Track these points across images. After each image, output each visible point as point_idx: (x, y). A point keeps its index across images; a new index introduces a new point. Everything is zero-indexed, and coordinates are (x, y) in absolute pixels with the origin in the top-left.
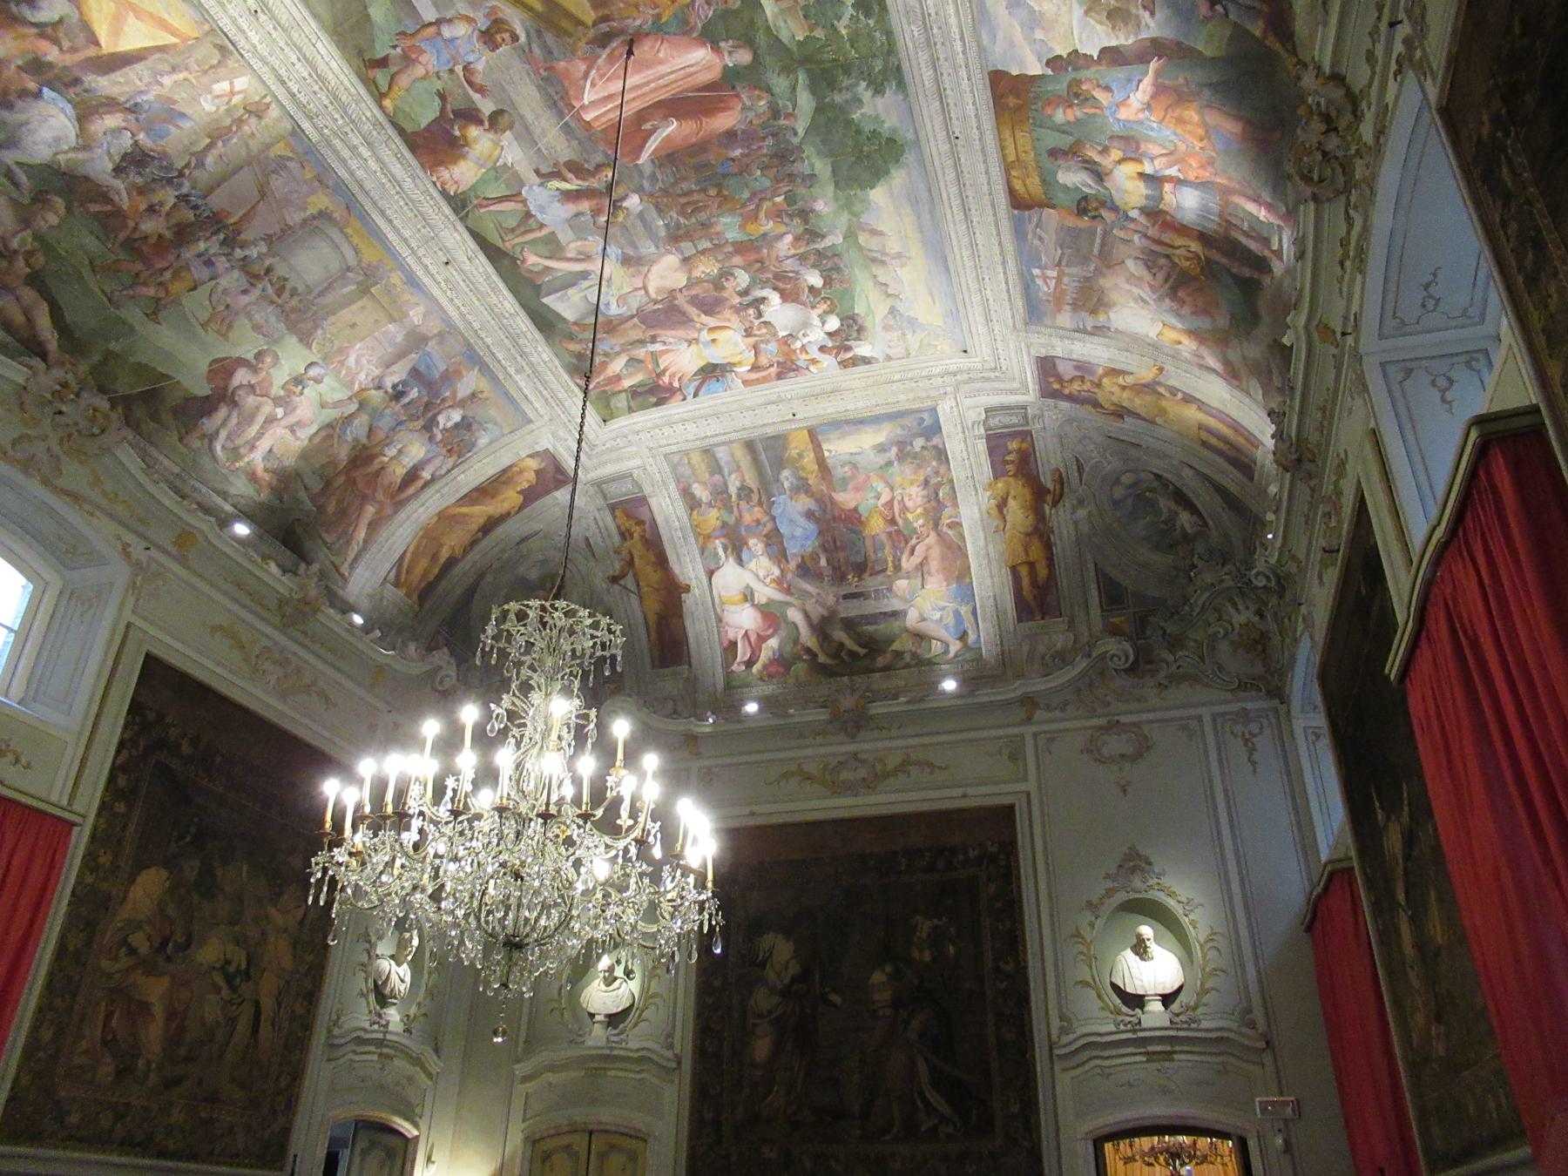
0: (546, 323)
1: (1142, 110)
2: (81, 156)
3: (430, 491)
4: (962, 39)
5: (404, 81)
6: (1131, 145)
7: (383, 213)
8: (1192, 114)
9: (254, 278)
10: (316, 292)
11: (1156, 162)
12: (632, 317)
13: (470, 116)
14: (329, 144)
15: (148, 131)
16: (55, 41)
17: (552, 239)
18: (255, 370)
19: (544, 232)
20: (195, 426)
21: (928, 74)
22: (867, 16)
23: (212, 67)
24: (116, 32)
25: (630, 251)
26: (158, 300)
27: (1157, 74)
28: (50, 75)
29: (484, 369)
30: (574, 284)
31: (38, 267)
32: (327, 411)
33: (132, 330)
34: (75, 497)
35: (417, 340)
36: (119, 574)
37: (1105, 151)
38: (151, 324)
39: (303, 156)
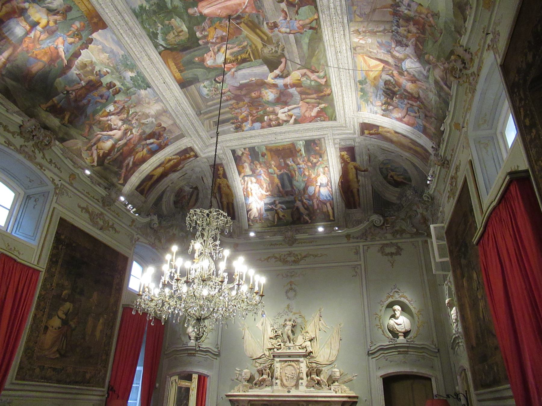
1: (57, 46)
4: (121, 34)
5: (307, 21)
6: (51, 32)
8: (45, 59)
11: (39, 33)
14: (342, 13)
16: (392, 73)
21: (127, 18)
22: (153, 32)
24: (377, 66)
26: (432, 16)
27: (62, 60)
37: (55, 22)
38: (441, 15)
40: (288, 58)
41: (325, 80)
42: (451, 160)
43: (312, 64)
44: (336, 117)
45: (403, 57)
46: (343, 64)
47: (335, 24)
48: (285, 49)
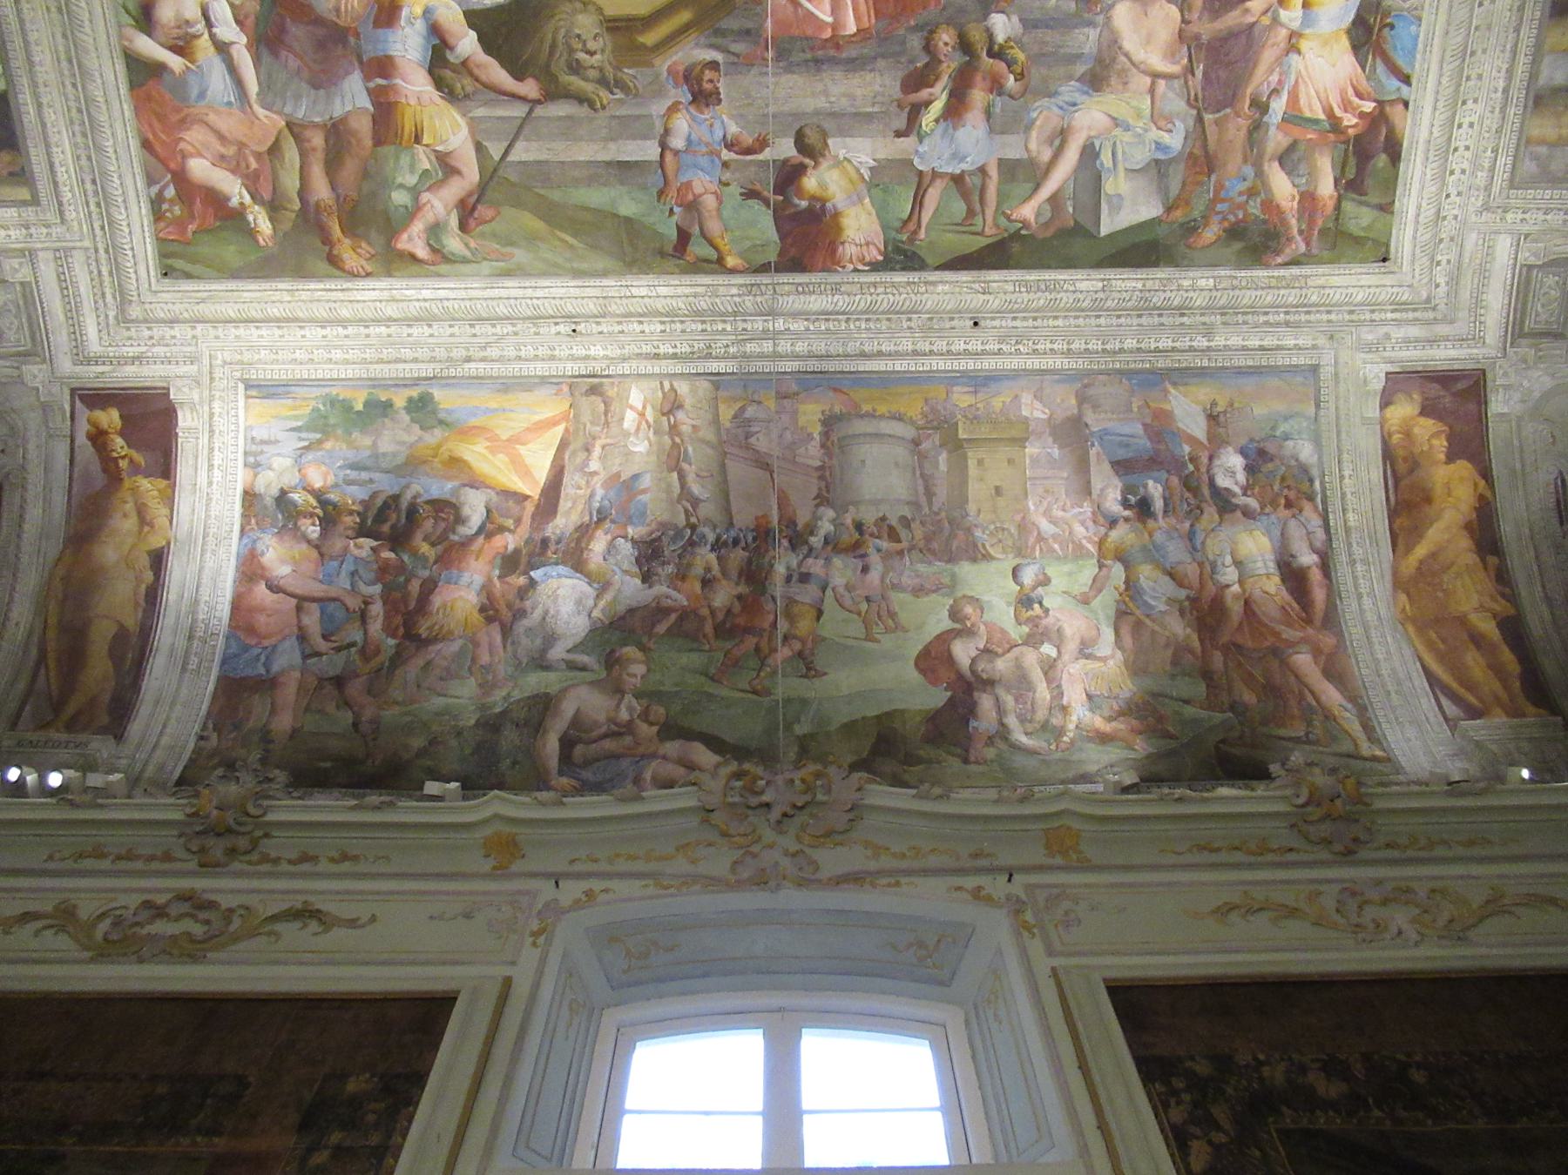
0: (1141, 250)
2: (608, 597)
3: (1342, 572)
5: (714, 227)
7: (864, 355)
9: (855, 549)
10: (923, 500)
12: (1200, 120)
13: (789, 176)
14: (745, 356)
15: (630, 520)
16: (502, 529)
17: (1009, 169)
18: (968, 632)
19: (993, 172)
20: (969, 738)
23: (606, 413)
24: (526, 473)
25: (1081, 69)
26: (800, 654)
28: (524, 560)
29: (1183, 376)
30: (1098, 179)
31: (662, 720)
32: (1096, 603)
33: (804, 702)
34: (855, 879)
35: (1072, 433)
36: (996, 929)
39: (747, 392)
40: (539, 111)
41: (422, 252)
42: (265, 859)
43: (508, 212)
44: (188, 276)
45: (592, 566)
46: (513, 339)
47: (700, 327)
48: (584, 111)
